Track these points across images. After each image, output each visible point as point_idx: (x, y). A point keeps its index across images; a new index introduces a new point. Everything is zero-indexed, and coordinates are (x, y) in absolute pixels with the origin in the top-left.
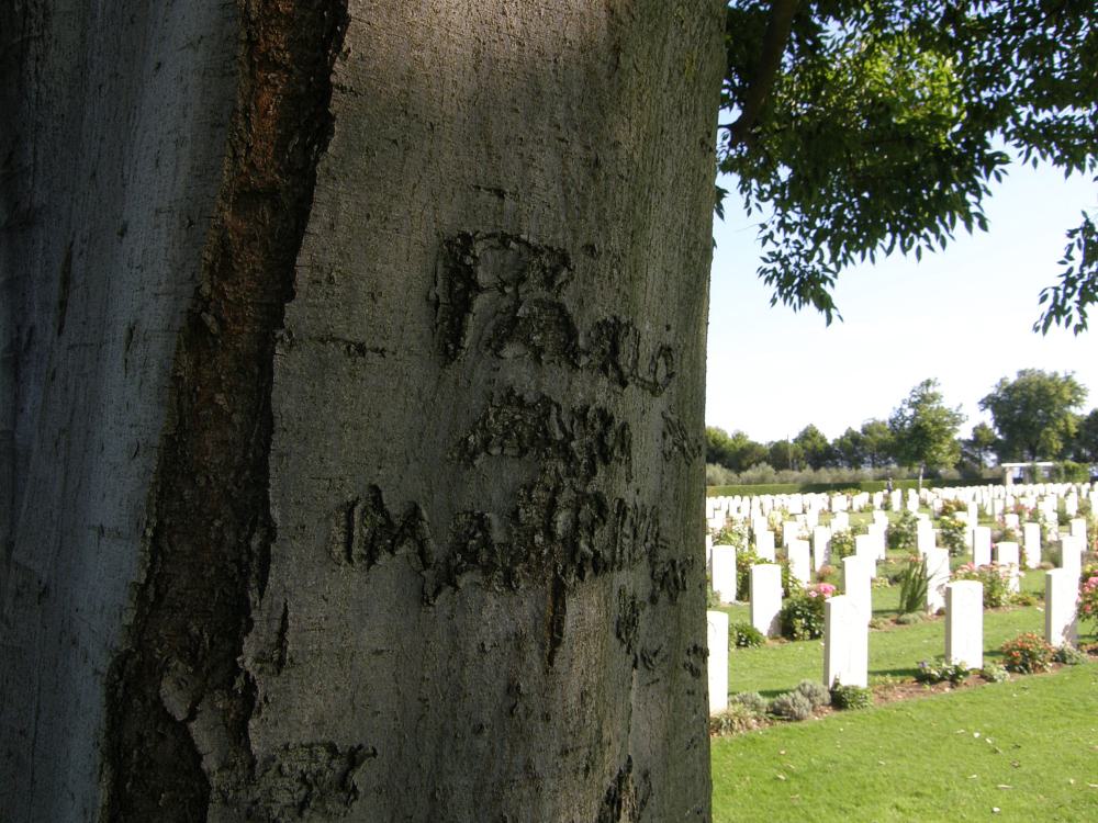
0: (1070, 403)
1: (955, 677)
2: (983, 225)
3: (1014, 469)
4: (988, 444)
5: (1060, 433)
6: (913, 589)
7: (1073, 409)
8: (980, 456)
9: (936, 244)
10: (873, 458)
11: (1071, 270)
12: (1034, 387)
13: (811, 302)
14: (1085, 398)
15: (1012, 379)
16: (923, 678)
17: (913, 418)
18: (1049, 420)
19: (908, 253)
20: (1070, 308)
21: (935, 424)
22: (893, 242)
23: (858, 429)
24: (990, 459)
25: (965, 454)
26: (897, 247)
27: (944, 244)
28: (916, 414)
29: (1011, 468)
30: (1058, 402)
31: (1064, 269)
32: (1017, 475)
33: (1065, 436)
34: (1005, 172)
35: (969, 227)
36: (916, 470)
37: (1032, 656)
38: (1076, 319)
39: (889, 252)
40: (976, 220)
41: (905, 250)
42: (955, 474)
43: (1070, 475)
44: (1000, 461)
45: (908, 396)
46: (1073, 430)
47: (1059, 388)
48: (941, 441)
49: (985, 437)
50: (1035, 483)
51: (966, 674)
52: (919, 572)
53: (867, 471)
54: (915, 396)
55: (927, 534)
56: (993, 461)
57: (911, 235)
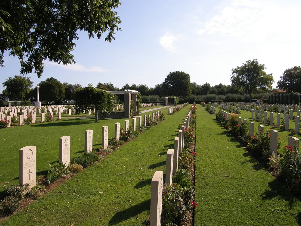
0: (28, 86)
13: (197, 85)
14: (32, 85)
15: (13, 77)
18: (21, 90)
23: (98, 84)
46: (28, 92)
52: (26, 118)
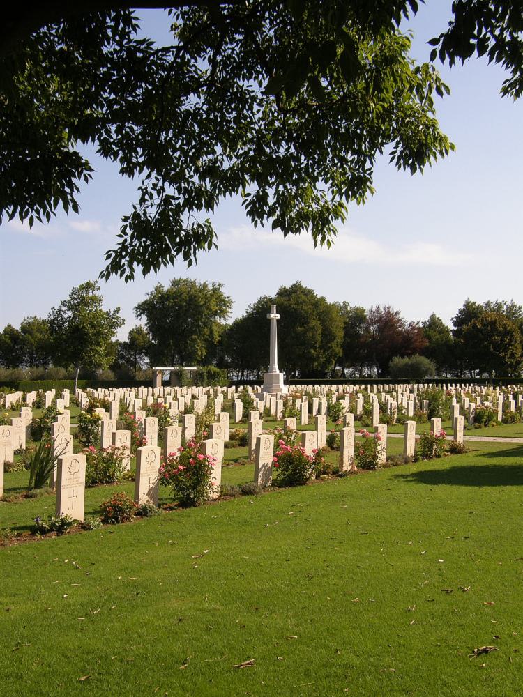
0: (216, 313)
1: (62, 527)
2: (76, 208)
3: (166, 371)
4: (143, 348)
5: (206, 340)
6: (41, 469)
7: (217, 318)
8: (136, 359)
9: (43, 217)
10: (31, 358)
11: (125, 241)
12: (185, 296)
14: (230, 310)
16: (36, 530)
17: (71, 320)
18: (195, 329)
19: (24, 220)
20: (124, 264)
21: (93, 326)
22: (14, 212)
23: (17, 326)
24: (144, 362)
25: (122, 357)
26: (17, 214)
27: (48, 217)
28: (75, 317)
29: (162, 371)
30: (206, 312)
31: (121, 240)
32: (167, 378)
33: (210, 343)
34: (91, 177)
35: (66, 209)
36: (71, 370)
37: (121, 511)
38: (127, 272)
39: (11, 217)
40: (71, 204)
41: (22, 218)
42: (110, 375)
43: (211, 379)
44: (152, 364)
45: (67, 298)
46: (217, 338)
47: (208, 299)
48: (98, 344)
49: (140, 342)
50: (181, 386)
51: (69, 524)
53: (25, 371)
54: (75, 299)
55: (63, 431)
56: (147, 364)
57: (27, 207)
